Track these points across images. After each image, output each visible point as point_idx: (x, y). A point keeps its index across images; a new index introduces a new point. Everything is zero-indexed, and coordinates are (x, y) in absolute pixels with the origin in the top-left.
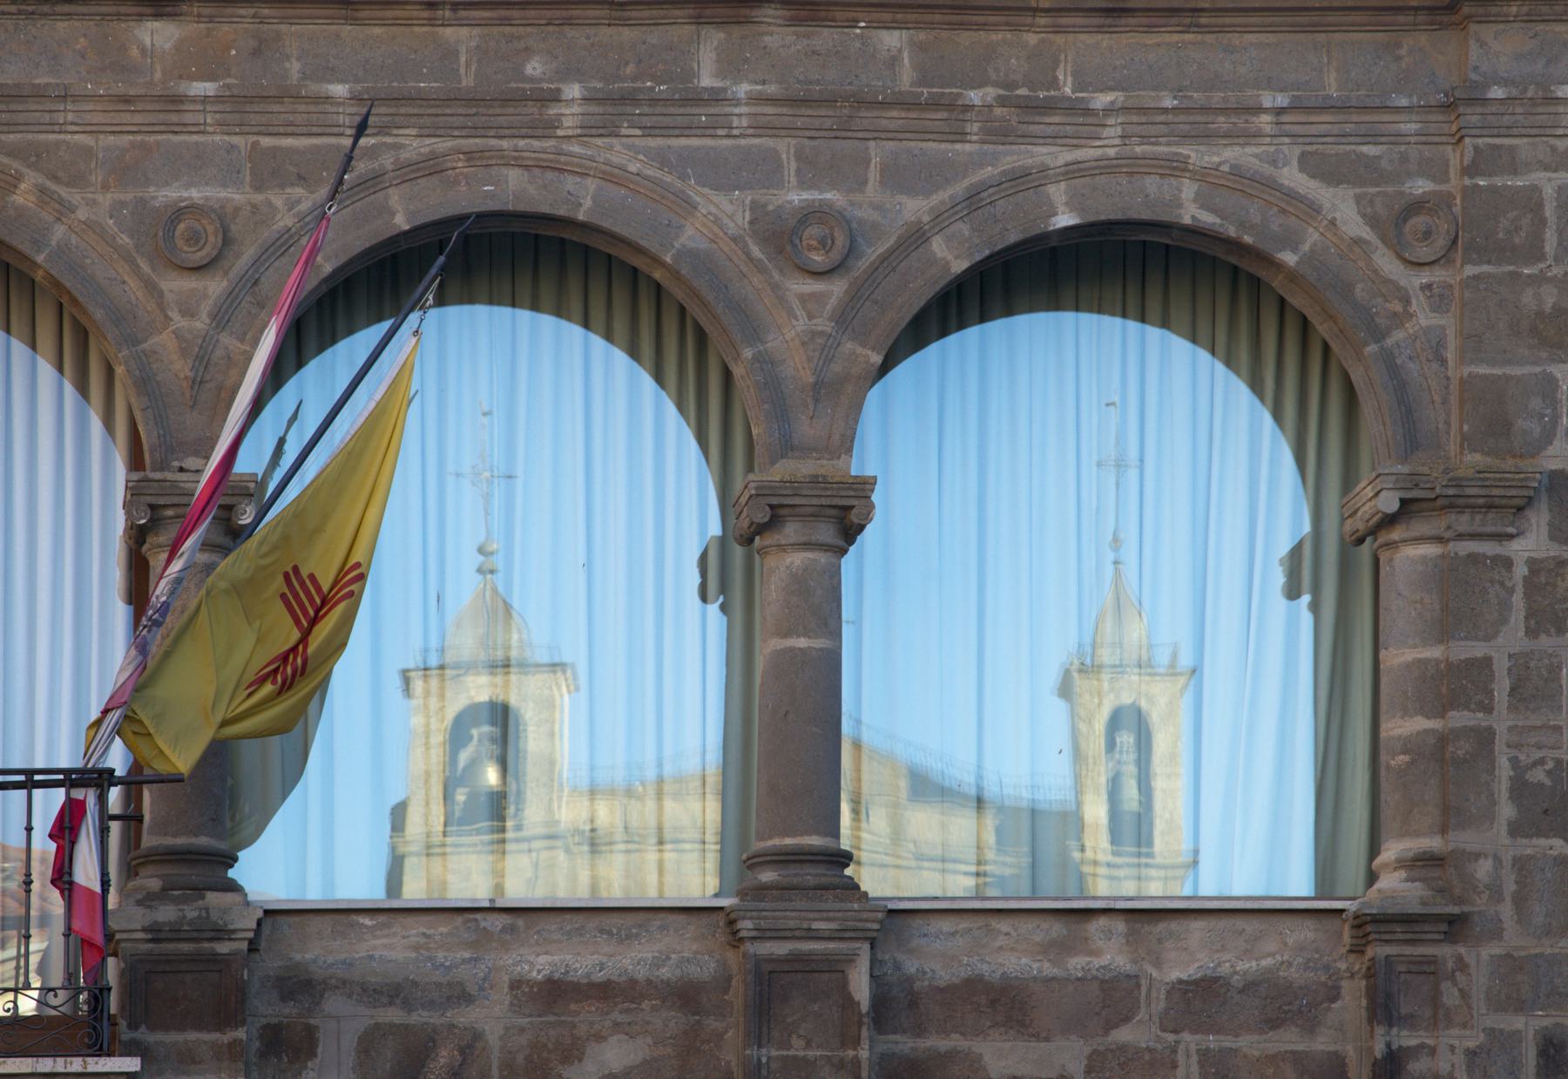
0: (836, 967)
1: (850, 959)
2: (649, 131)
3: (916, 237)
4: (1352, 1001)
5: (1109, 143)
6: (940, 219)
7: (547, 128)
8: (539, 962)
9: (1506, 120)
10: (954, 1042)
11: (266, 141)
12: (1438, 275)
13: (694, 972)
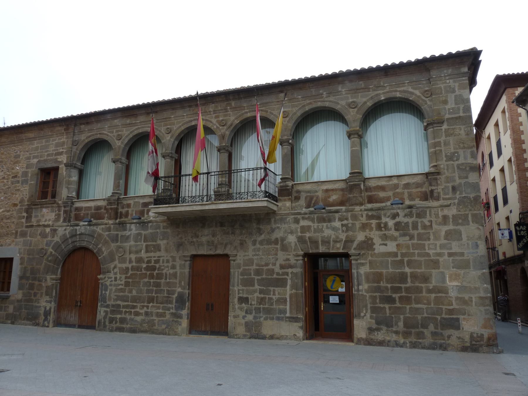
0: (359, 185)
1: (361, 184)
2: (334, 96)
3: (365, 103)
4: (427, 184)
5: (387, 89)
6: (368, 100)
7: (322, 97)
8: (325, 187)
9: (436, 79)
10: (376, 193)
11: (292, 103)
12: (430, 98)
13: (343, 187)
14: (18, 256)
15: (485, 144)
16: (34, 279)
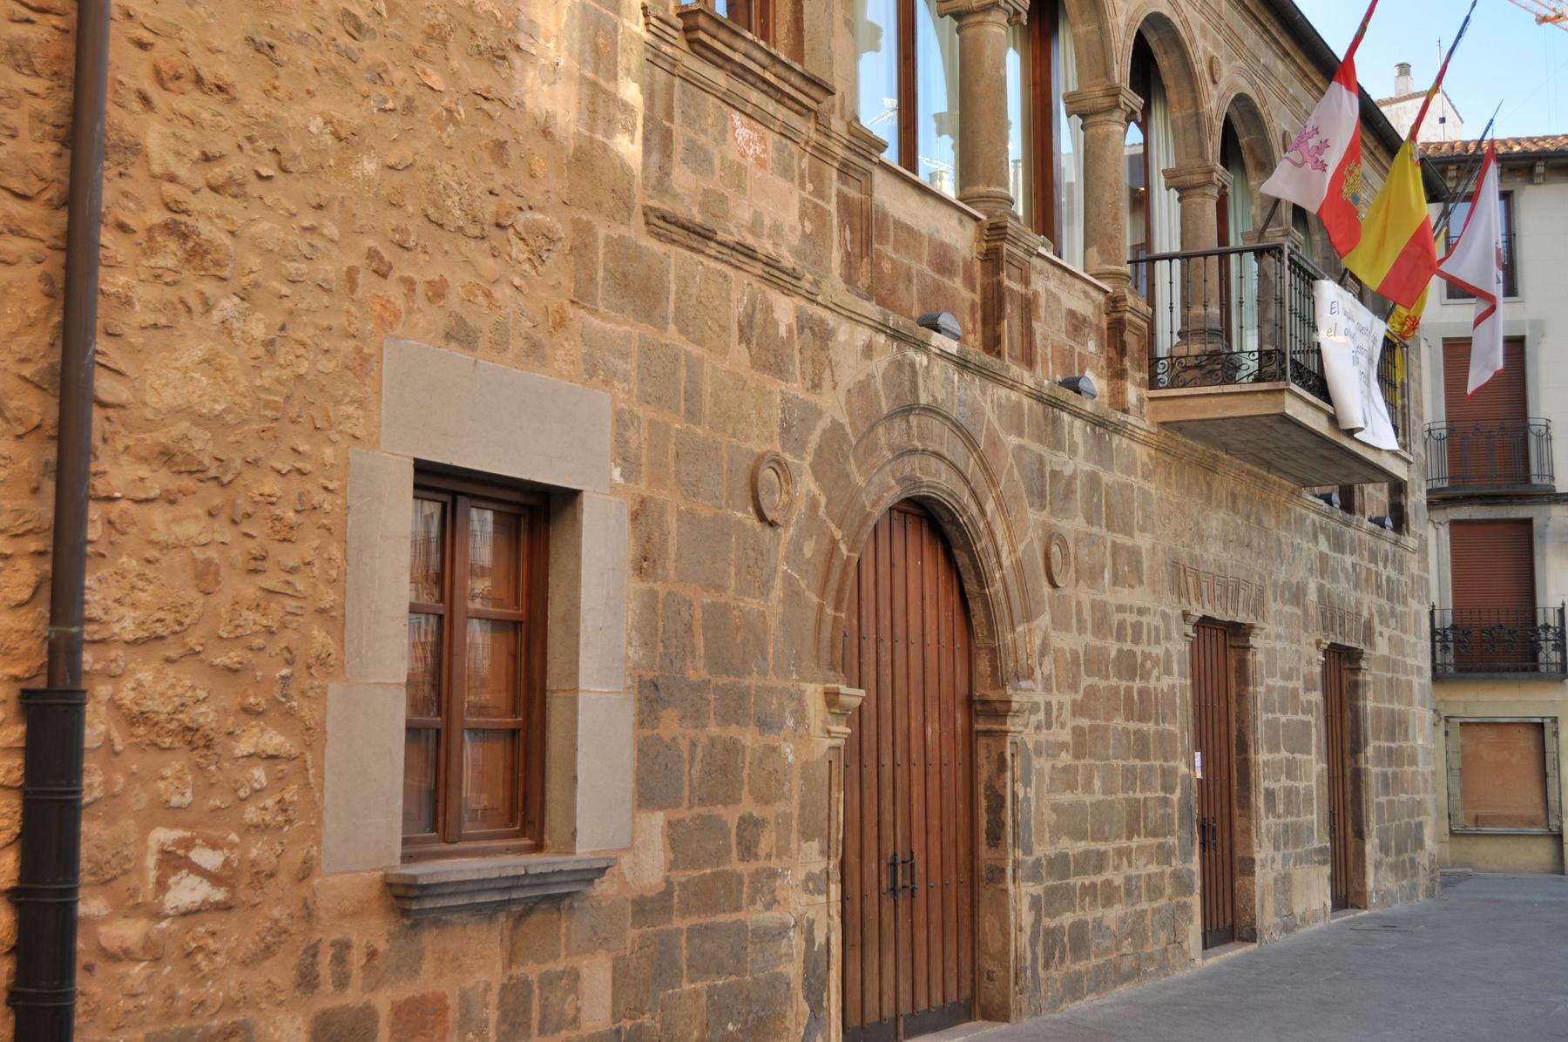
14: (614, 488)
15: (934, 822)
16: (735, 707)
